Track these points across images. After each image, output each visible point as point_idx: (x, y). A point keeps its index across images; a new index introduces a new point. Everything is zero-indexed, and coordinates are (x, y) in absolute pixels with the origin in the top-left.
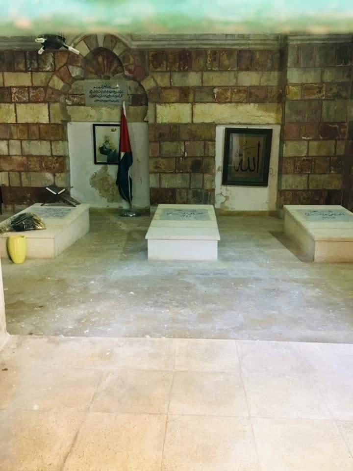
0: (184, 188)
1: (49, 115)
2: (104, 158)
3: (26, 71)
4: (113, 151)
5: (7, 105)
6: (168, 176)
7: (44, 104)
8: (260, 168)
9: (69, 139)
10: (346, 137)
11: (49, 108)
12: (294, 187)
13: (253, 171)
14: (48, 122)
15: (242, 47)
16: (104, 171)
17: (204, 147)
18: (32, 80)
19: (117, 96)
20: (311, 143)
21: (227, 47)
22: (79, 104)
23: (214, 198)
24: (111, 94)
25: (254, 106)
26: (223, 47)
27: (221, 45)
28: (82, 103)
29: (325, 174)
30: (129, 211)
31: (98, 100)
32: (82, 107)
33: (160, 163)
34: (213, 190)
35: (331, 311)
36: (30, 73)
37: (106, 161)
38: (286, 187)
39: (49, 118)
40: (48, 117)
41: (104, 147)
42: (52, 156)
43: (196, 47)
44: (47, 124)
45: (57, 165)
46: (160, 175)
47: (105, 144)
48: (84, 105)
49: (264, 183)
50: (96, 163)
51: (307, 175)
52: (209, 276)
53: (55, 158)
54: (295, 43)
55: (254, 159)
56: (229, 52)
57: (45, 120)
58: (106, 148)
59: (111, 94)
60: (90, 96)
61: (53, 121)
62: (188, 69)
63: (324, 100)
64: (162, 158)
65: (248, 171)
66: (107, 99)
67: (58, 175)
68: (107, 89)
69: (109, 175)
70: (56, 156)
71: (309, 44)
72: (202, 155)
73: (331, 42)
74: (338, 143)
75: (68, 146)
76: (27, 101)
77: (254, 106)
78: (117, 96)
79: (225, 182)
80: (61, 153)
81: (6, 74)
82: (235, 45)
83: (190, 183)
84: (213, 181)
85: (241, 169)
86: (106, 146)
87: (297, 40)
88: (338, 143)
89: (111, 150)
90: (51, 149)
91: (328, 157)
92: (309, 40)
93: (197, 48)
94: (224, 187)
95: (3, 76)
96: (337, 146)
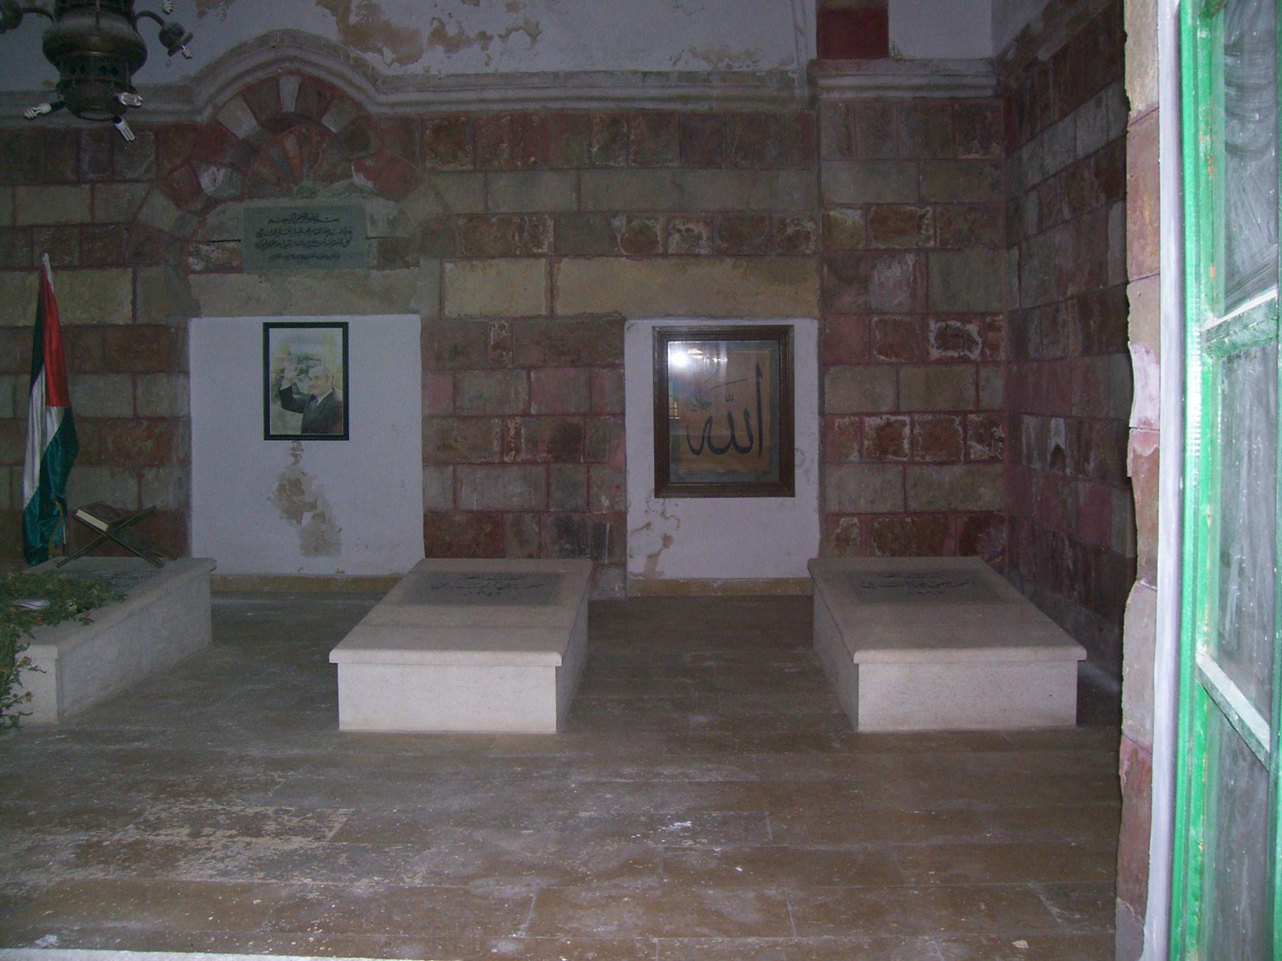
0: (528, 512)
1: (134, 302)
2: (294, 422)
3: (77, 183)
4: (320, 400)
5: (18, 275)
6: (480, 474)
7: (120, 270)
8: (766, 443)
9: (192, 371)
10: (1002, 356)
11: (134, 283)
12: (862, 502)
13: (747, 450)
14: (130, 322)
15: (690, 107)
16: (292, 459)
17: (590, 384)
18: (92, 207)
19: (334, 243)
20: (904, 372)
21: (649, 105)
22: (225, 268)
23: (625, 542)
24: (319, 238)
25: (735, 267)
26: (637, 105)
27: (631, 99)
28: (235, 263)
29: (953, 463)
30: (200, 242)
31: (278, 256)
32: (233, 277)
33: (454, 433)
34: (621, 517)
35: (1108, 926)
36: (88, 186)
37: (299, 433)
38: (840, 503)
39: (134, 309)
40: (130, 307)
41: (294, 390)
42: (137, 418)
43: (558, 105)
44: (127, 326)
45: (149, 444)
46: (455, 471)
47: (296, 380)
48: (239, 270)
49: (783, 485)
50: (268, 436)
51: (901, 468)
52: (408, 754)
53: (145, 423)
54: (835, 95)
55: (746, 414)
56: (658, 121)
57: (122, 316)
58: (299, 393)
59: (319, 238)
60: (257, 245)
61: (142, 319)
62: (535, 162)
63: (933, 250)
64: (464, 419)
65: (732, 450)
66: (306, 252)
67: (150, 474)
68: (305, 226)
69: (304, 474)
70: (146, 418)
71: (876, 100)
72: (583, 410)
73: (939, 94)
74: (984, 372)
75: (187, 391)
76: (76, 263)
77: (735, 267)
78: (334, 243)
79: (664, 485)
80: (163, 409)
81: (22, 191)
82: (671, 99)
83: (548, 494)
84: (621, 488)
85: (711, 447)
86: (299, 384)
87: (843, 89)
88: (984, 372)
89: (313, 398)
90: (135, 397)
91: (956, 413)
92: (878, 88)
93: (563, 109)
94: (657, 503)
95: (14, 196)
96: (982, 383)
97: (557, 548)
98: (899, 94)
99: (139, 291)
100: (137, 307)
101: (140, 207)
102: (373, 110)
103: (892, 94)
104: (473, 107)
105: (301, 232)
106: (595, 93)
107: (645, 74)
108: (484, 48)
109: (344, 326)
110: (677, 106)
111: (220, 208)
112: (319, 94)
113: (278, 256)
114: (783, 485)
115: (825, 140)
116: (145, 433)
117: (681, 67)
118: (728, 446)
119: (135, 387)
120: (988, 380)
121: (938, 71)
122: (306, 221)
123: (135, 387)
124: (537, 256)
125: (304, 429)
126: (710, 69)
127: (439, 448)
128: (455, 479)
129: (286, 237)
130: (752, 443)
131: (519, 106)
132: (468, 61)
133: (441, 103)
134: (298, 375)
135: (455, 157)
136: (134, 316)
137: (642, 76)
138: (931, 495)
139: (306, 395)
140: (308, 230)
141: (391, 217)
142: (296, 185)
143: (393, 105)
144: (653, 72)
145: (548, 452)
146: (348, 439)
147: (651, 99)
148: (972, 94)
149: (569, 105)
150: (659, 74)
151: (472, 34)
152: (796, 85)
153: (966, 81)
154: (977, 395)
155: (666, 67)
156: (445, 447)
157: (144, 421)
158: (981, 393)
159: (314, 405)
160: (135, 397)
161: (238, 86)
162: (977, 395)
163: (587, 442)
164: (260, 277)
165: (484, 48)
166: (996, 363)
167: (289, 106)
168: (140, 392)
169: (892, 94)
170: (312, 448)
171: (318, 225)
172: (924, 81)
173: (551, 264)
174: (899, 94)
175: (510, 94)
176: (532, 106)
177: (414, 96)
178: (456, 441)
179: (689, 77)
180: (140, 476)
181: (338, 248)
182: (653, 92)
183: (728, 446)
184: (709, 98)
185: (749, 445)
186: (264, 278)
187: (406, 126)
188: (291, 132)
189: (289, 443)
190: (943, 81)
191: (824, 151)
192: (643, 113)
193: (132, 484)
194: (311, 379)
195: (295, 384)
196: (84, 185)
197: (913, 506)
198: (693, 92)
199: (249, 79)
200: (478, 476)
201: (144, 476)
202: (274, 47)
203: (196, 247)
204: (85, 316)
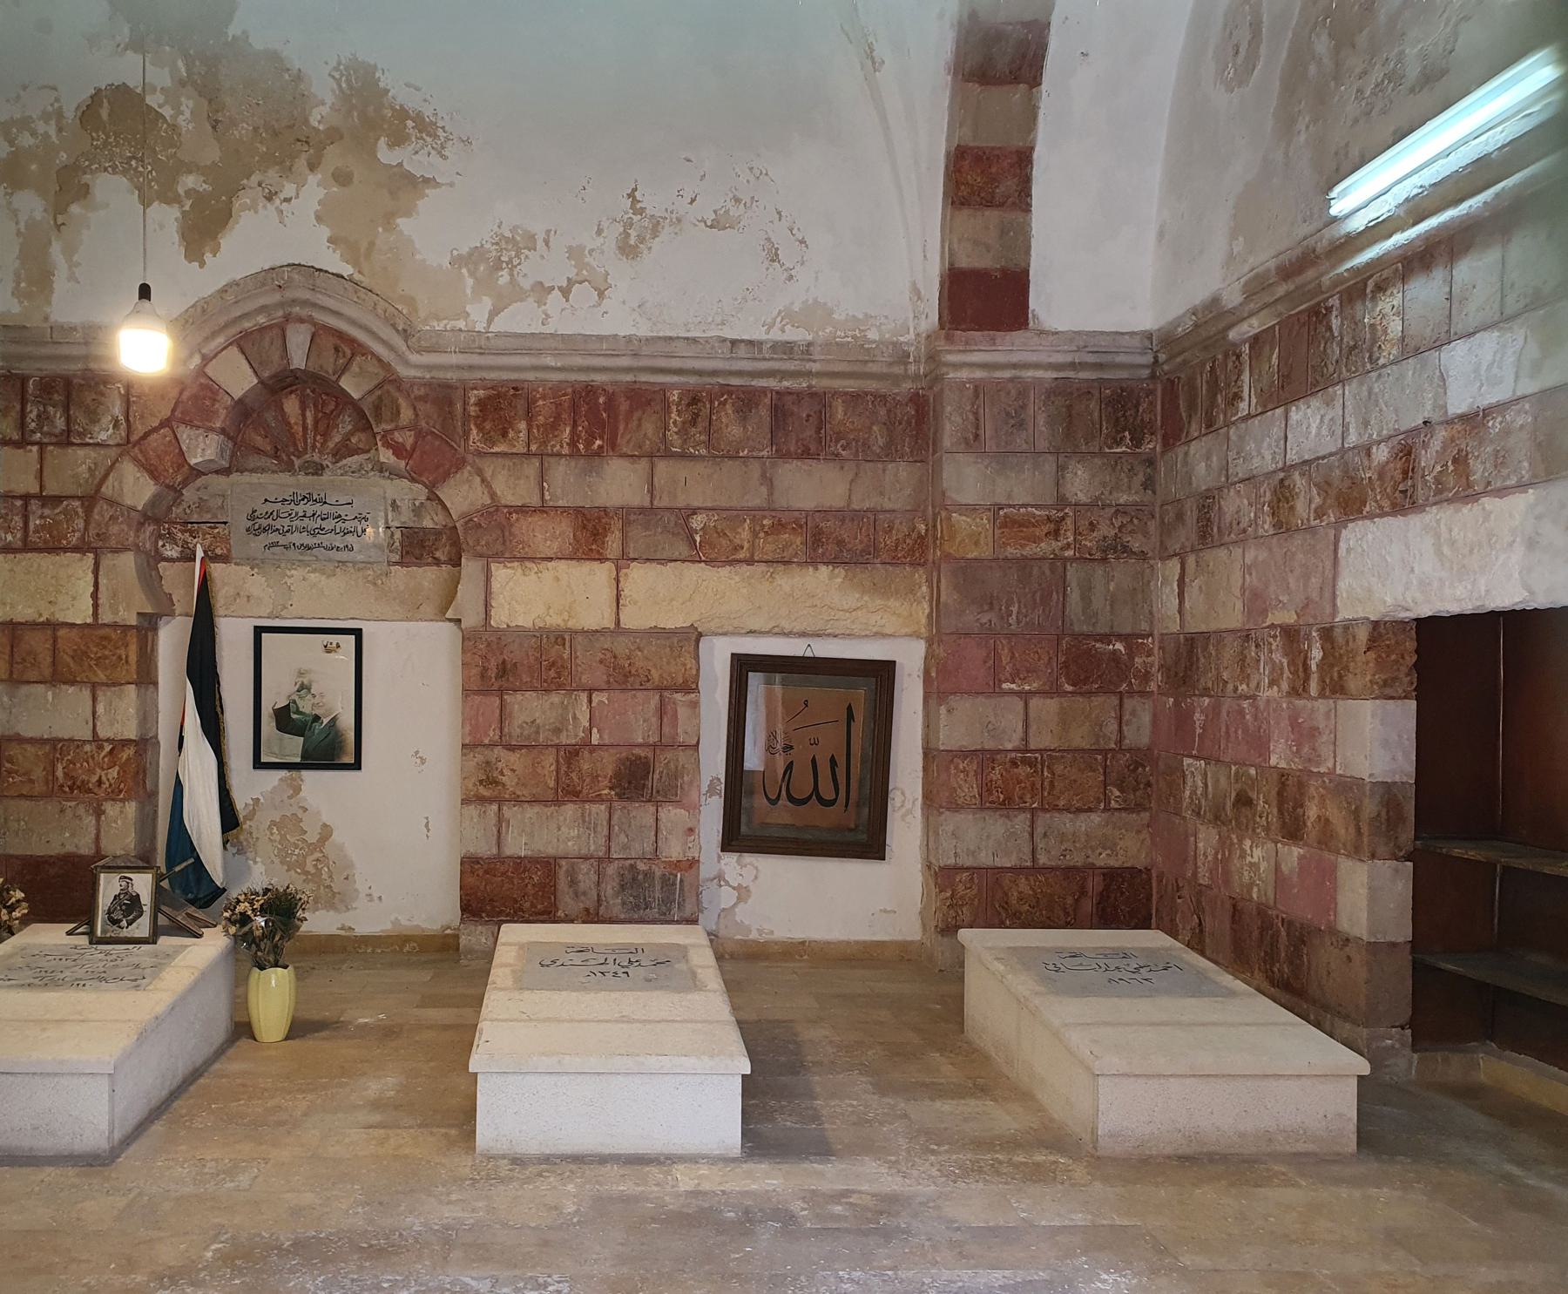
1: (95, 596)
2: (293, 747)
4: (325, 721)
6: (532, 812)
7: (78, 555)
12: (983, 854)
13: (832, 803)
14: (89, 620)
17: (661, 711)
31: (275, 544)
36: (35, 449)
37: (298, 760)
39: (96, 606)
43: (629, 378)
45: (114, 773)
49: (870, 845)
54: (964, 374)
56: (746, 400)
57: (80, 613)
58: (298, 712)
61: (106, 617)
62: (601, 447)
68: (310, 508)
71: (1012, 380)
72: (651, 741)
73: (1084, 375)
86: (300, 703)
88: (1129, 704)
89: (317, 718)
91: (1099, 751)
92: (1014, 366)
97: (619, 901)
98: (1039, 374)
99: (103, 581)
100: (100, 602)
101: (106, 476)
102: (404, 372)
103: (1030, 373)
104: (530, 376)
105: (304, 516)
106: (675, 364)
107: (734, 342)
108: (540, 302)
109: (358, 633)
110: (772, 383)
111: (200, 482)
112: (337, 349)
113: (275, 544)
114: (870, 845)
115: (948, 428)
116: (106, 759)
117: (776, 335)
118: (810, 798)
119: (94, 700)
120: (1133, 713)
121: (1086, 347)
122: (311, 503)
123: (94, 700)
124: (602, 560)
125: (305, 754)
126: (810, 338)
127: (481, 782)
128: (500, 819)
129: (286, 522)
130: (837, 794)
131: (583, 377)
132: (520, 319)
133: (491, 368)
134: (298, 691)
135: (504, 435)
136: (95, 614)
137: (729, 345)
138: (1063, 848)
139: (309, 715)
140: (314, 515)
141: (417, 503)
142: (298, 457)
143: (429, 368)
144: (742, 341)
145: (611, 788)
146: (360, 768)
147: (740, 373)
148: (1124, 374)
149: (643, 378)
150: (751, 343)
151: (526, 284)
152: (911, 360)
153: (1121, 359)
154: (1120, 731)
155: (758, 334)
156: (490, 782)
157: (106, 744)
158: (1124, 728)
159: (317, 727)
160: (94, 713)
161: (233, 331)
162: (1120, 731)
163: (656, 776)
164: (252, 569)
165: (540, 302)
166: (1143, 694)
167: (298, 361)
168: (100, 709)
169: (1030, 373)
170: (315, 782)
171: (326, 509)
172: (1069, 358)
173: (618, 569)
174: (1039, 374)
175: (579, 361)
176: (599, 378)
177: (455, 359)
178: (502, 773)
179: (787, 348)
180: (99, 813)
181: (350, 539)
182: (747, 366)
183: (810, 798)
184: (809, 374)
185: (834, 797)
186: (256, 570)
187: (442, 395)
188: (291, 393)
189: (283, 773)
190: (1091, 359)
191: (947, 442)
192: (727, 390)
193: (89, 821)
194: (314, 696)
195: (294, 702)
196: (29, 447)
197: (1043, 860)
198: (791, 366)
199: (247, 325)
200: (528, 816)
201: (104, 812)
202: (280, 287)
203: (169, 529)
204: (30, 611)
